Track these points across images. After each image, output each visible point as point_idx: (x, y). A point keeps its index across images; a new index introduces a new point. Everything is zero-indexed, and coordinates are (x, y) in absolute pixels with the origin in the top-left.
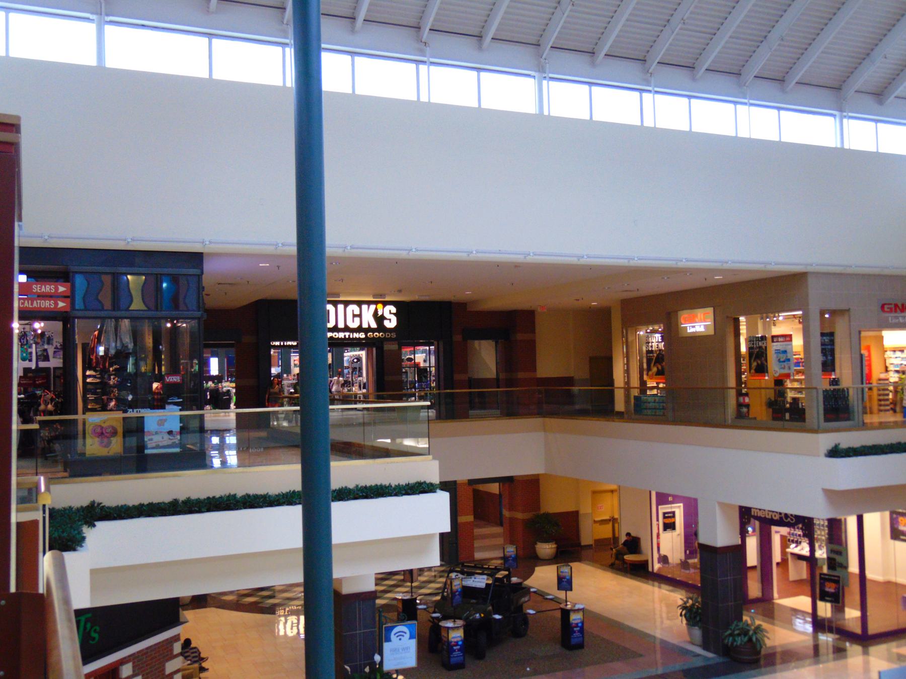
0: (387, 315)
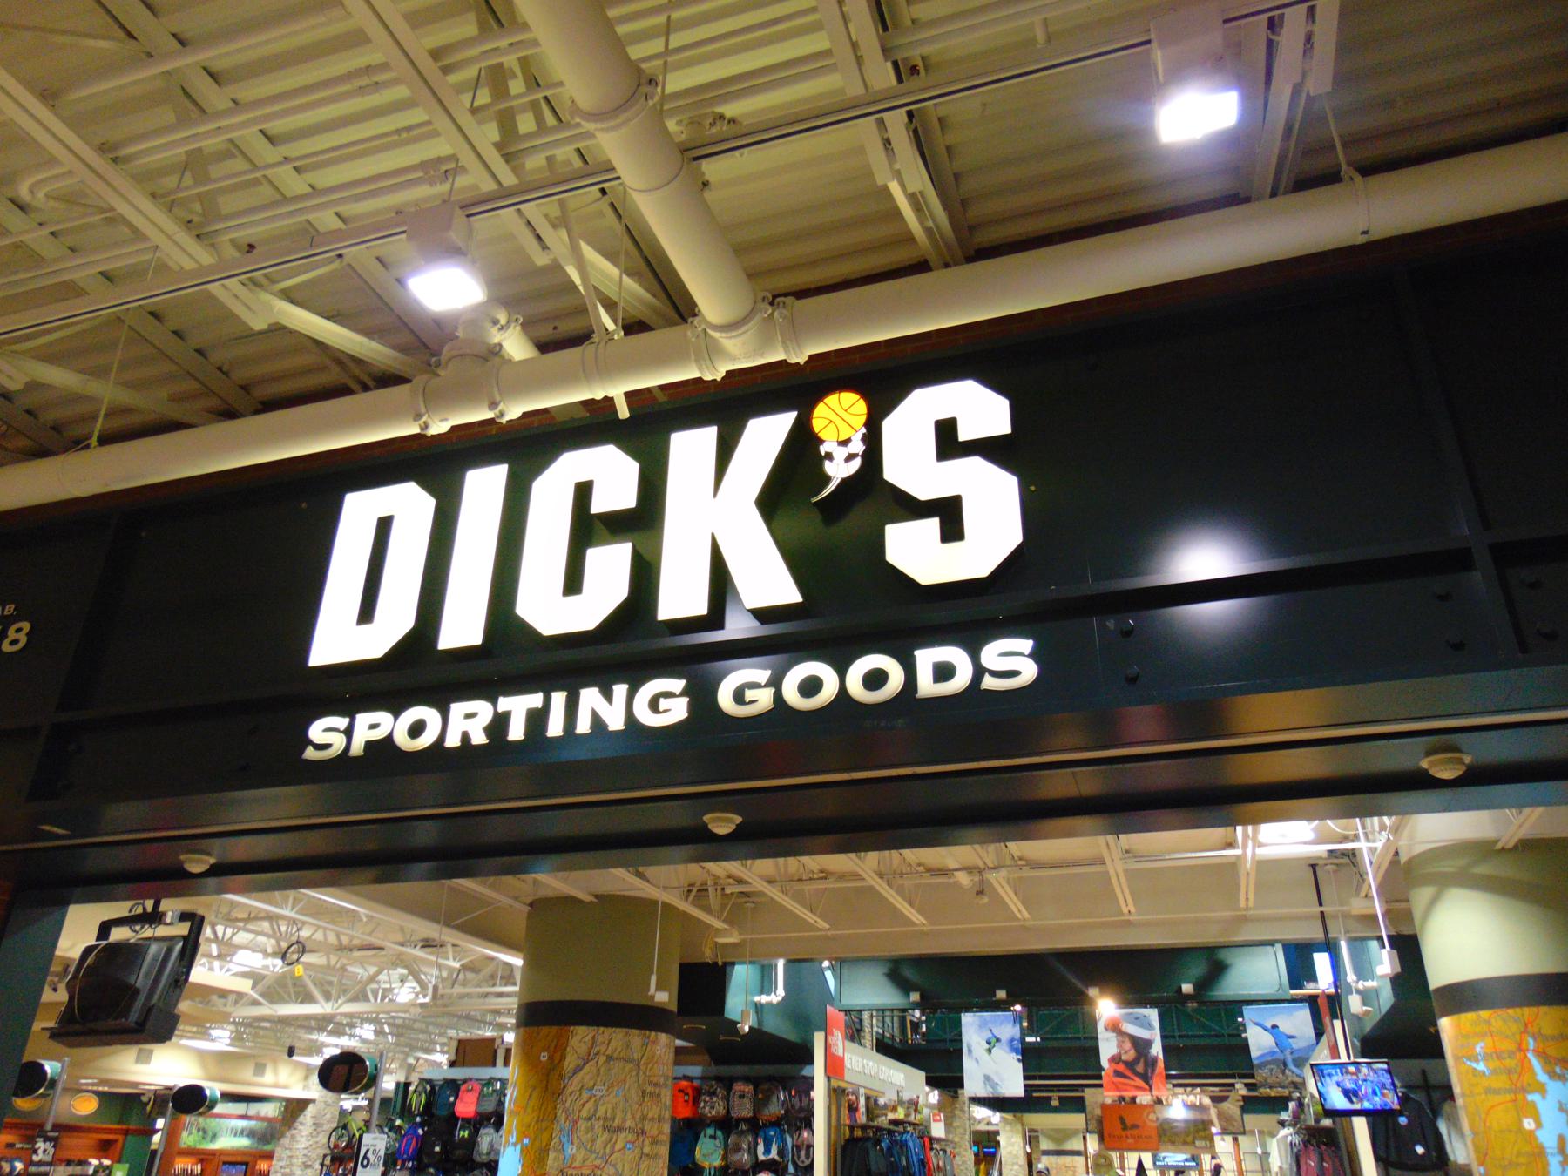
0: (910, 464)
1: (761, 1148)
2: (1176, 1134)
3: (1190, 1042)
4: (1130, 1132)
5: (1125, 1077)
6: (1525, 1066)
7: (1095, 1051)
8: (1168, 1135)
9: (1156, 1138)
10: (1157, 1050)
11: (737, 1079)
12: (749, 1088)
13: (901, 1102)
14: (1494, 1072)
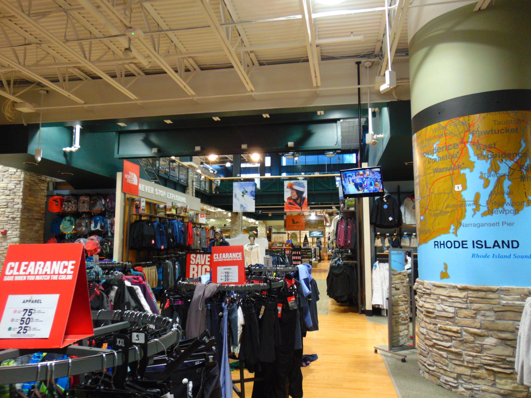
1: (93, 225)
2: (311, 225)
3: (317, 192)
4: (295, 224)
5: (293, 205)
6: (464, 152)
7: (283, 195)
8: (309, 225)
9: (304, 226)
10: (305, 195)
11: (82, 195)
12: (87, 199)
13: (173, 207)
14: (442, 158)
